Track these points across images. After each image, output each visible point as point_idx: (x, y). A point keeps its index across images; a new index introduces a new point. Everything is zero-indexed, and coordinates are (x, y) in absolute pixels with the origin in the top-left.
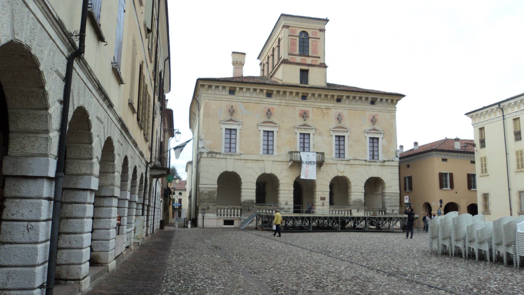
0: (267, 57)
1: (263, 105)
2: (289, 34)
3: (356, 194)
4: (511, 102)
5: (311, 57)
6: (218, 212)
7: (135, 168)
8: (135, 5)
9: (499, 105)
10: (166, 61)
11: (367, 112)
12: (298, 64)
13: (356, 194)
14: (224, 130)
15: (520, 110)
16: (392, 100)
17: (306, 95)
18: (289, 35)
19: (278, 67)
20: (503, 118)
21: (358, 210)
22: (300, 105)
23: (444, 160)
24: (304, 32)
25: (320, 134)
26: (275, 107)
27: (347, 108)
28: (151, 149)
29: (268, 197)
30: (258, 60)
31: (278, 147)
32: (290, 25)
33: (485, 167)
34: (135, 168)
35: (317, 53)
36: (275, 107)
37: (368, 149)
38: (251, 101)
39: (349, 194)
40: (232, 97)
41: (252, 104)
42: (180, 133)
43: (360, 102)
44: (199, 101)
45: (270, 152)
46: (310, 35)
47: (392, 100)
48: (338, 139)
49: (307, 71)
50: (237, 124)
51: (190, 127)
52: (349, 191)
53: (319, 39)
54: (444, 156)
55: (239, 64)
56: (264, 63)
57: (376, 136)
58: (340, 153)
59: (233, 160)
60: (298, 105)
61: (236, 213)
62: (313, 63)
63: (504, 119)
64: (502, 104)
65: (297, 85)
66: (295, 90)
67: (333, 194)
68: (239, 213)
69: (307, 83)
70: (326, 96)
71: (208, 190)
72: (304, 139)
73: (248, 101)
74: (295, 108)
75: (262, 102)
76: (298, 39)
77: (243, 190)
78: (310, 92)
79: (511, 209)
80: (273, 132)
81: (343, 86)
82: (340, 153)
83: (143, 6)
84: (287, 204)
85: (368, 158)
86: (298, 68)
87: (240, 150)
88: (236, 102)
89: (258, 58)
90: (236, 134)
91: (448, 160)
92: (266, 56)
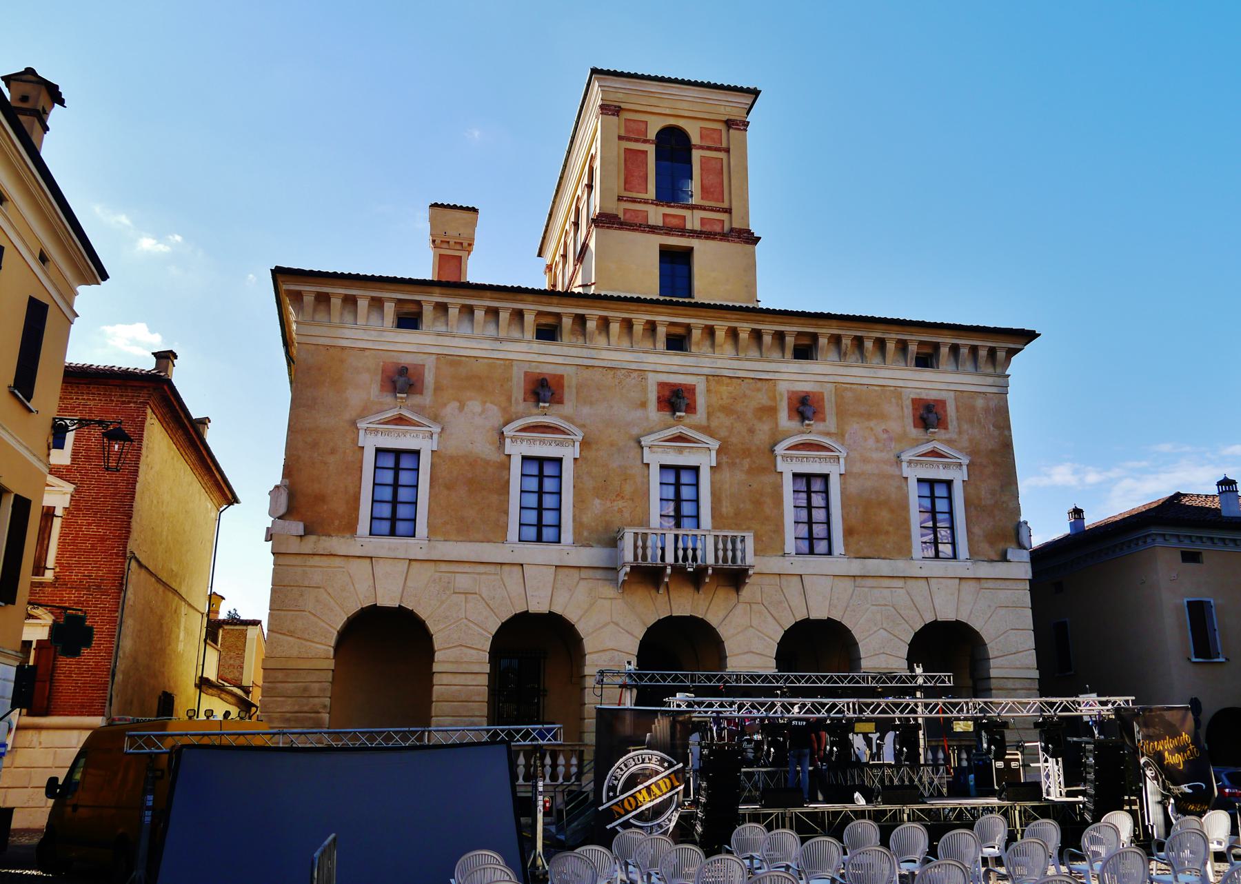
2: (623, 133)
12: (653, 229)
16: (992, 352)
18: (620, 138)
23: (1191, 557)
32: (623, 105)
43: (853, 358)
45: (548, 533)
47: (992, 352)
48: (926, 492)
50: (831, 457)
54: (1187, 541)
55: (452, 243)
61: (561, 769)
66: (640, 318)
69: (690, 295)
78: (697, 322)
80: (558, 461)
86: (657, 240)
90: (417, 470)
91: (1205, 556)
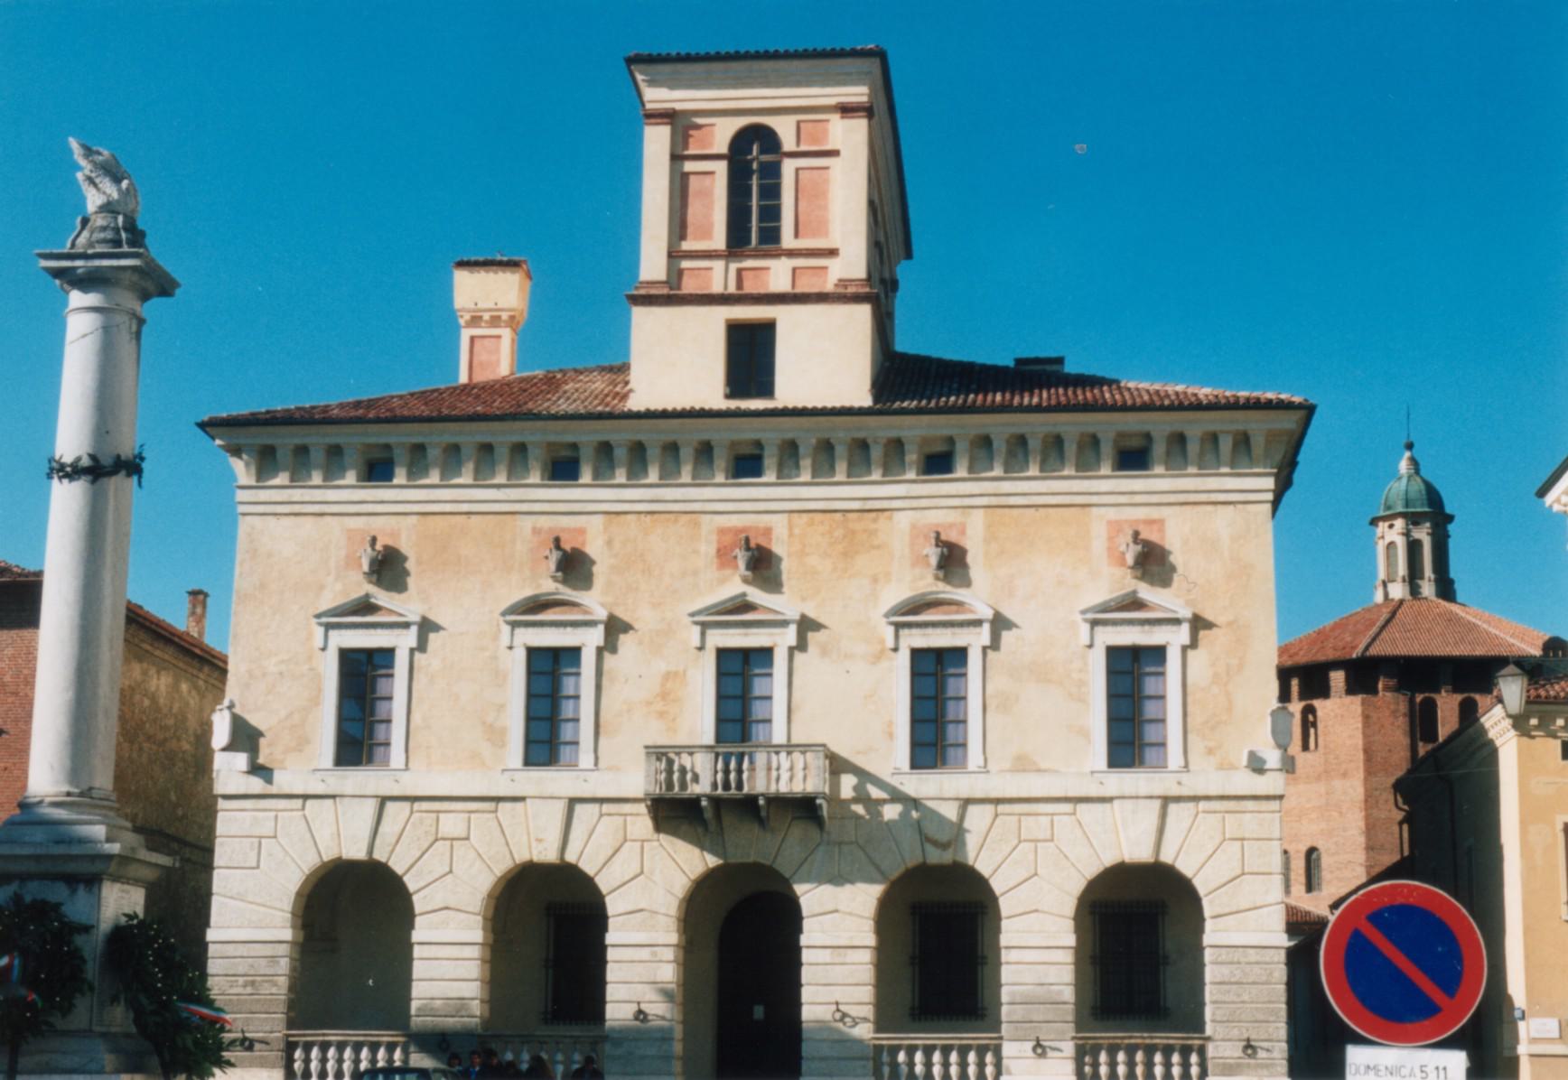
1: (527, 523)
3: (230, 950)
5: (792, 253)
6: (882, 1064)
11: (1094, 510)
13: (230, 950)
17: (756, 452)
35: (821, 228)
36: (779, 524)
46: (788, 144)
49: (766, 331)
53: (834, 153)
62: (805, 286)
67: (984, 957)
70: (985, 443)
74: (697, 525)
76: (721, 168)
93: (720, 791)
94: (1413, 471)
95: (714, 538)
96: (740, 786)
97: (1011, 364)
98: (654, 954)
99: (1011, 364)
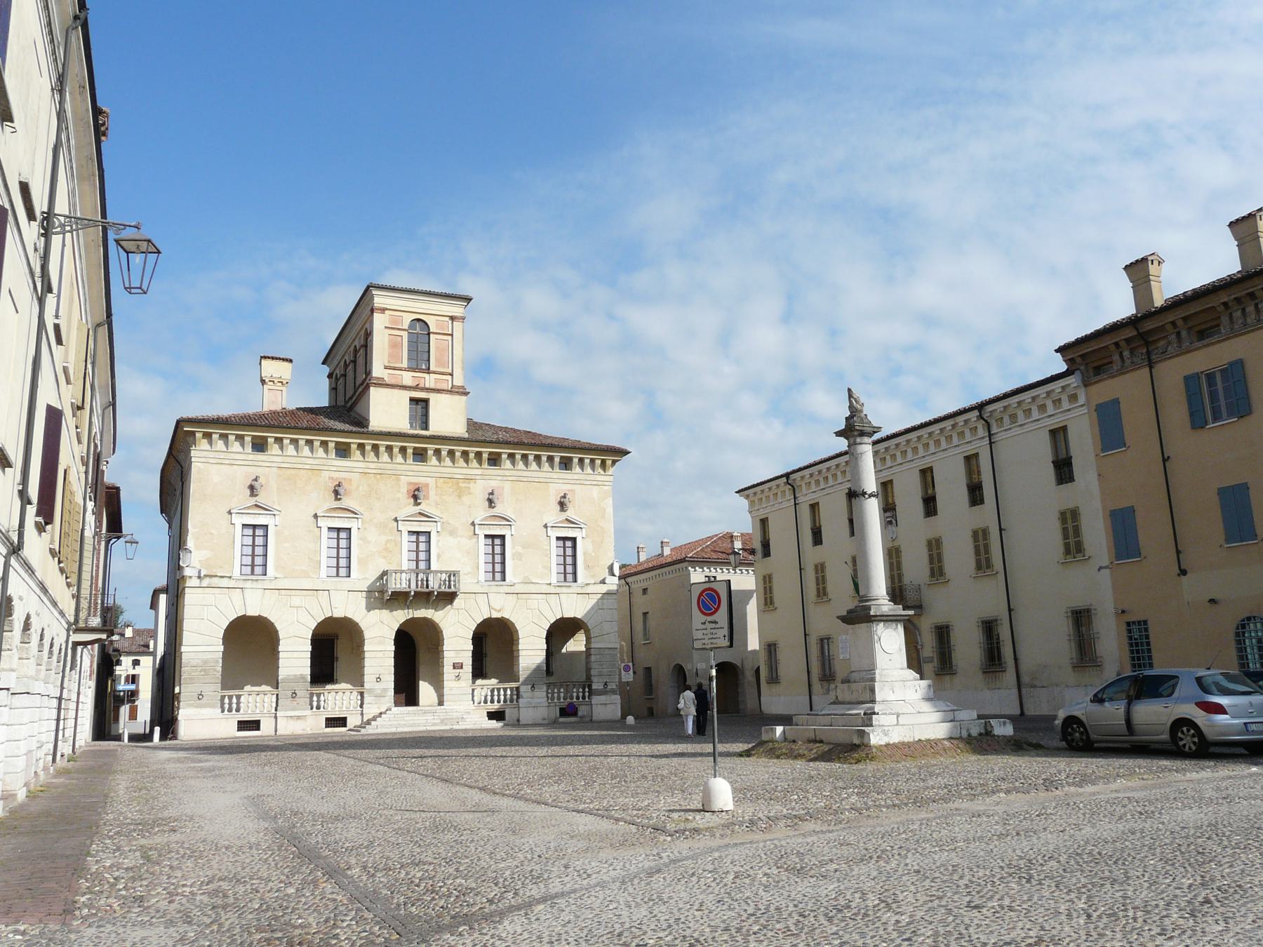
0: (342, 363)
4: (923, 433)
5: (435, 373)
7: (28, 617)
8: (54, 376)
9: (788, 479)
10: (106, 411)
14: (239, 528)
15: (1045, 415)
19: (363, 391)
20: (990, 440)
21: (533, 686)
22: (409, 473)
24: (419, 320)
25: (452, 533)
26: (355, 477)
27: (510, 478)
28: (77, 597)
29: (340, 668)
30: (325, 366)
31: (360, 560)
33: (771, 593)
34: (28, 617)
37: (554, 560)
38: (300, 466)
39: (515, 654)
40: (260, 457)
41: (302, 471)
42: (137, 543)
44: (183, 463)
49: (426, 402)
51: (164, 509)
52: (514, 647)
56: (337, 374)
57: (570, 534)
58: (498, 569)
59: (260, 592)
60: (404, 473)
63: (991, 443)
64: (792, 476)
65: (403, 431)
68: (587, 694)
71: (201, 656)
72: (417, 542)
73: (295, 466)
74: (398, 480)
75: (326, 468)
76: (405, 334)
77: (281, 655)
79: (808, 672)
81: (506, 430)
82: (498, 569)
83: (62, 345)
84: (379, 679)
85: (554, 581)
86: (409, 394)
87: (277, 568)
88: (267, 469)
89: (324, 363)
92: (360, 330)
93: (419, 589)
94: (750, 569)
95: (406, 486)
96: (427, 587)
97: (845, 614)
98: (384, 654)
99: (845, 614)
